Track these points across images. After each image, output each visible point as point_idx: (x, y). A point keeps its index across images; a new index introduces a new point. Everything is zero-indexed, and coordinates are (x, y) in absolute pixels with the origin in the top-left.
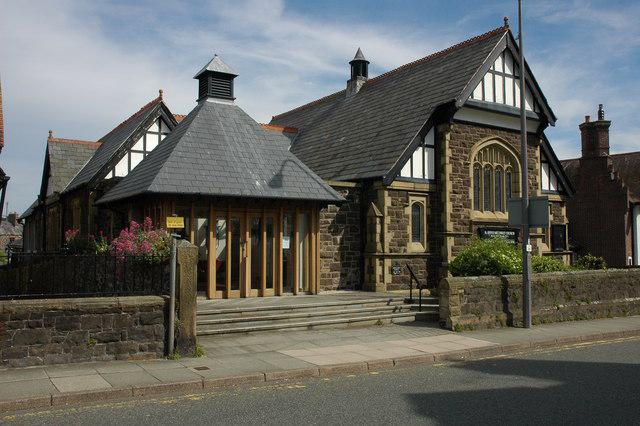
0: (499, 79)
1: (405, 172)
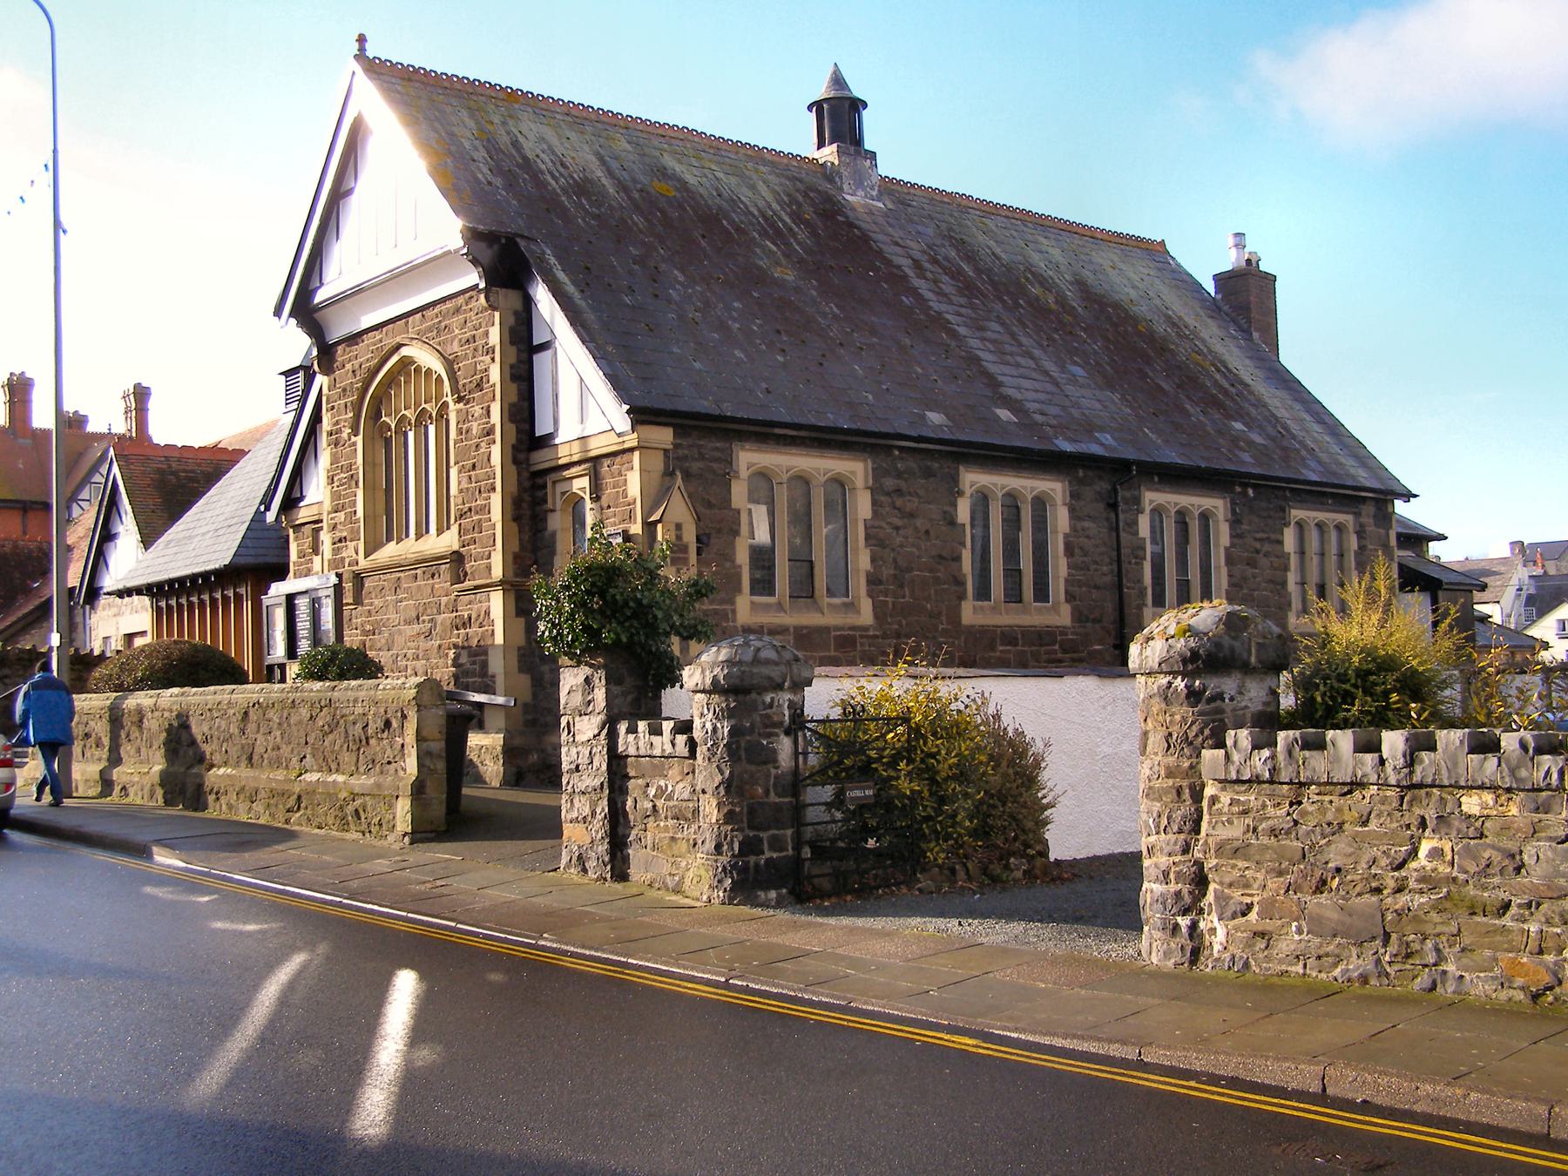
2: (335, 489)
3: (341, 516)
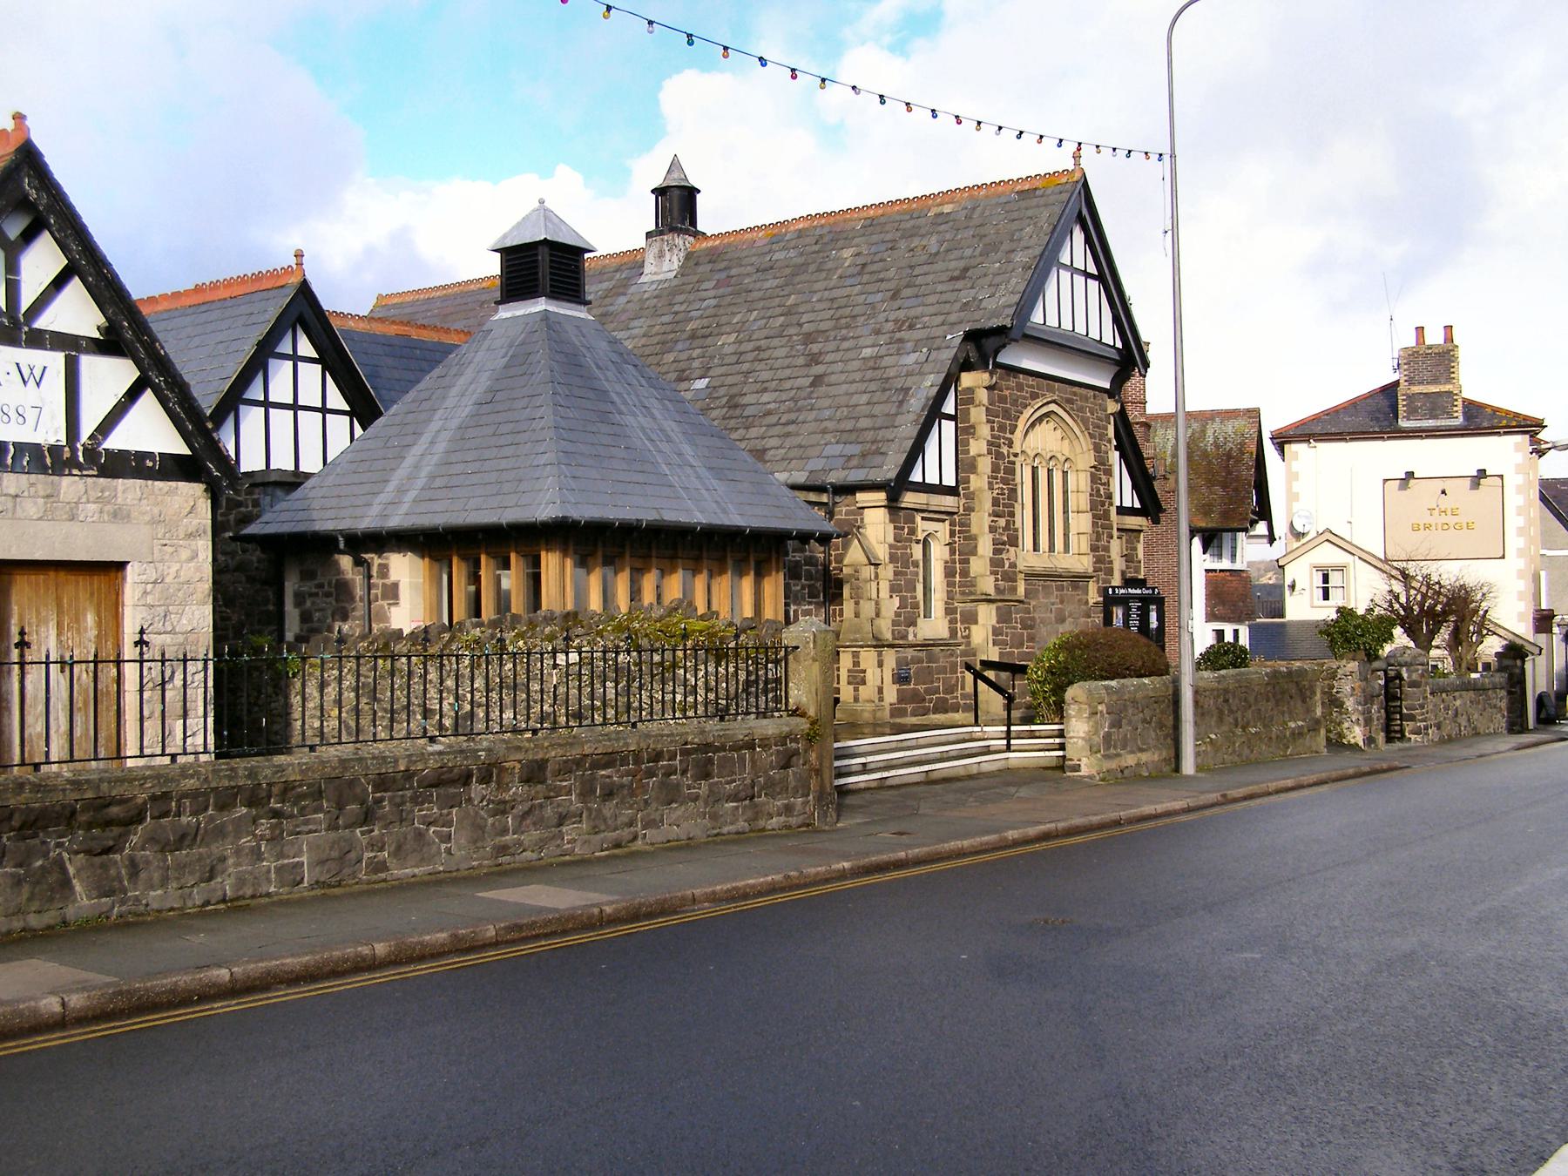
0: (1079, 280)
1: (916, 476)
2: (995, 495)
3: (1002, 522)
